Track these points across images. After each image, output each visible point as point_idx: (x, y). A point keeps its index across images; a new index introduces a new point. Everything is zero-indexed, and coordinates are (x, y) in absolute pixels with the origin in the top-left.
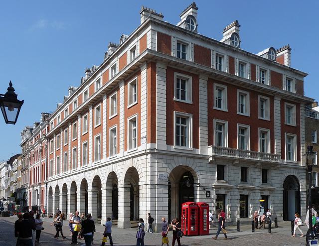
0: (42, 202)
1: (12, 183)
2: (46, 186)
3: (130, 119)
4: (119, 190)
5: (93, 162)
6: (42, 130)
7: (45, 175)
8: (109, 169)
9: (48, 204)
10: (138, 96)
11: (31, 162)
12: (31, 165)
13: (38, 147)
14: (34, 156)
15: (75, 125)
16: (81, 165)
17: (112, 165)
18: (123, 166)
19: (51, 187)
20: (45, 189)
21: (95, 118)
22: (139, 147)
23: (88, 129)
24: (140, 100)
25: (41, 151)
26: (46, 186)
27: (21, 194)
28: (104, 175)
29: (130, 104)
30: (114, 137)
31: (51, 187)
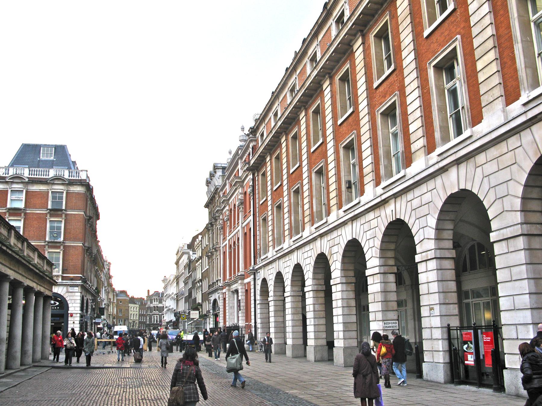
0: (247, 318)
1: (194, 283)
2: (255, 279)
3: (343, 146)
4: (370, 280)
5: (377, 184)
6: (241, 158)
7: (253, 252)
8: (346, 234)
9: (259, 321)
10: (394, 57)
11: (224, 234)
12: (224, 239)
13: (237, 198)
14: (229, 219)
15: (295, 137)
16: (340, 206)
17: (295, 253)
18: (309, 254)
19: (264, 281)
20: (252, 287)
21: (312, 134)
22: (408, 170)
23: (325, 136)
24: (399, 61)
25: (243, 203)
26: (255, 279)
27: (209, 303)
28: (287, 270)
29: (442, 12)
30: (352, 162)
31: (264, 281)
